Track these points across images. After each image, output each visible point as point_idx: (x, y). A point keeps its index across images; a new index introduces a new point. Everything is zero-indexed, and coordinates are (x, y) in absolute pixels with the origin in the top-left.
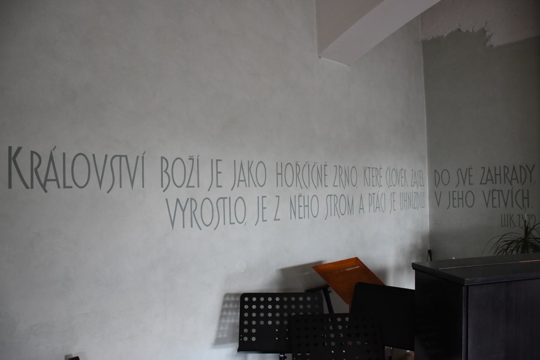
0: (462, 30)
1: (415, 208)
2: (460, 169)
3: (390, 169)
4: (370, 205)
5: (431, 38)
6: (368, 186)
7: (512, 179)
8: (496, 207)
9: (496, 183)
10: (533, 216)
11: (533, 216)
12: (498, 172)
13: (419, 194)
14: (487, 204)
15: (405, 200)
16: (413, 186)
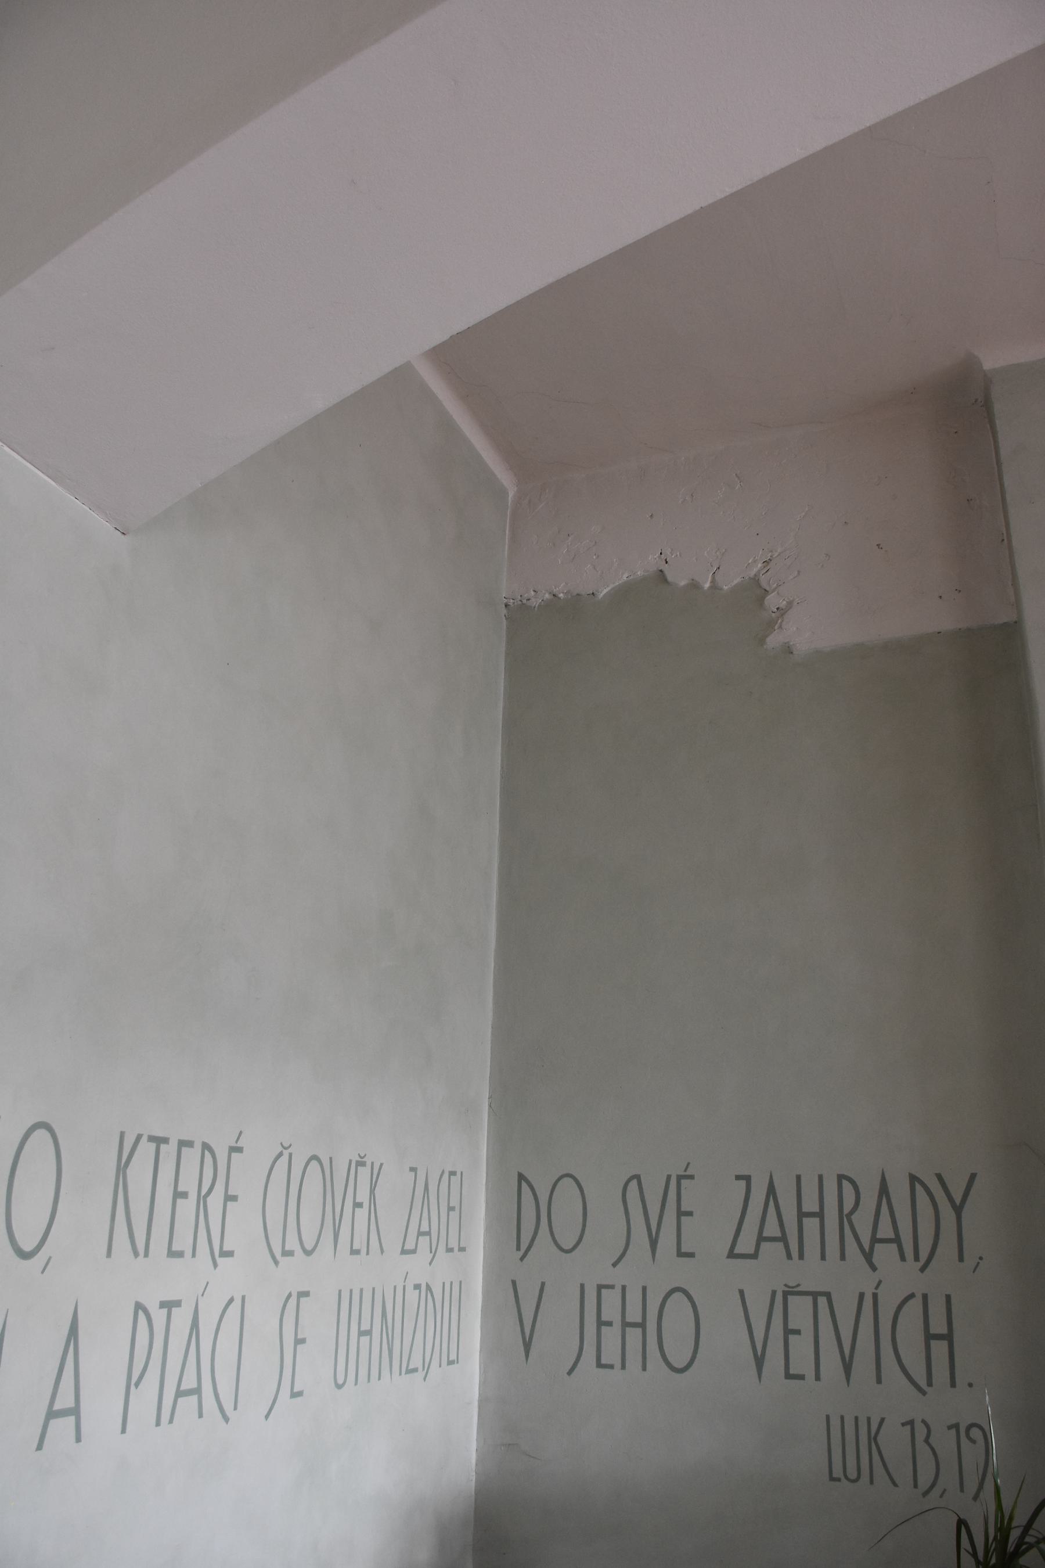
0: (670, 578)
1: (415, 1370)
2: (637, 1177)
3: (290, 1155)
4: (132, 1382)
5: (547, 596)
6: (136, 1254)
7: (875, 1240)
8: (801, 1377)
9: (801, 1256)
10: (975, 1433)
11: (975, 1433)
12: (810, 1205)
13: (437, 1291)
14: (759, 1362)
15: (361, 1333)
16: (414, 1251)
